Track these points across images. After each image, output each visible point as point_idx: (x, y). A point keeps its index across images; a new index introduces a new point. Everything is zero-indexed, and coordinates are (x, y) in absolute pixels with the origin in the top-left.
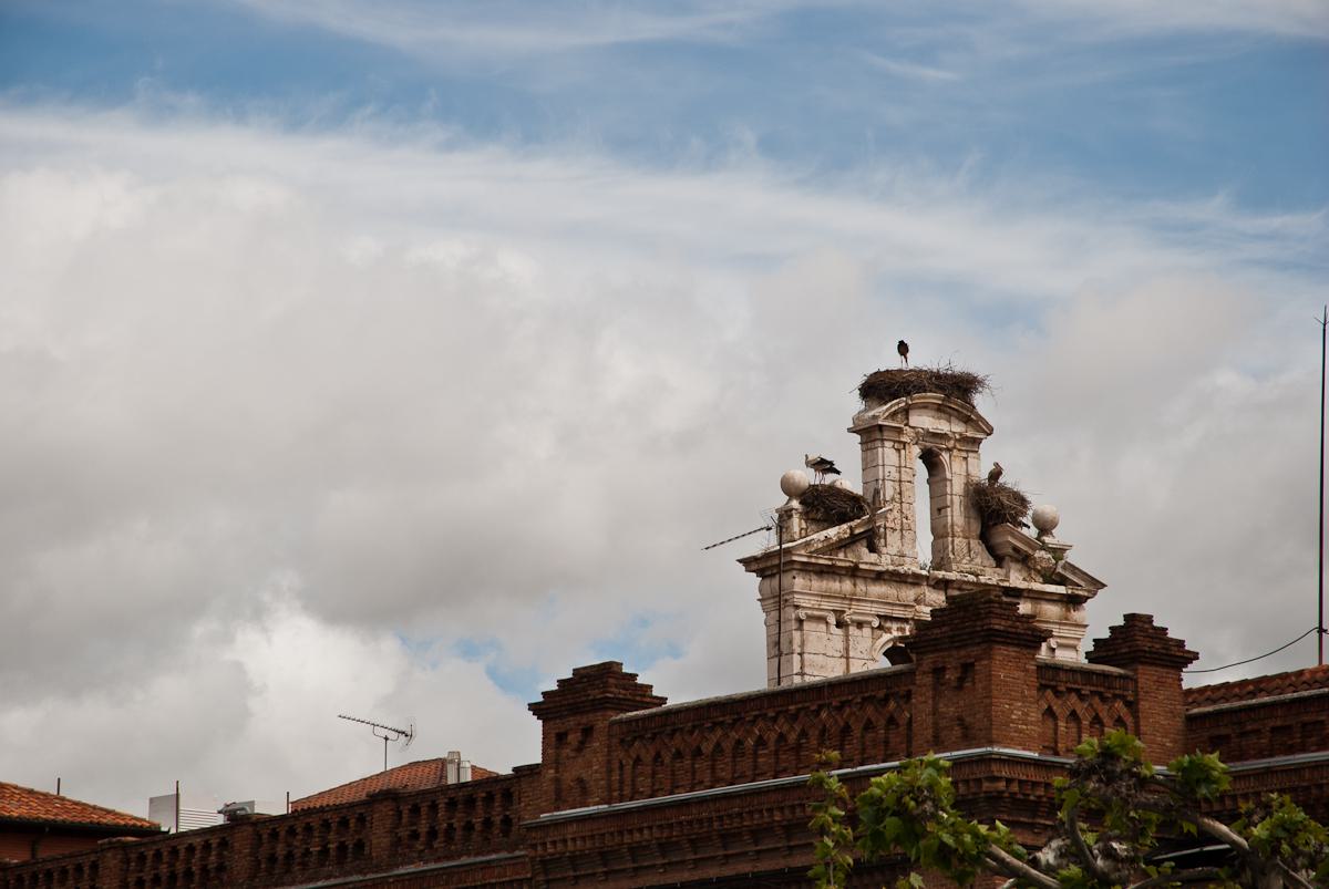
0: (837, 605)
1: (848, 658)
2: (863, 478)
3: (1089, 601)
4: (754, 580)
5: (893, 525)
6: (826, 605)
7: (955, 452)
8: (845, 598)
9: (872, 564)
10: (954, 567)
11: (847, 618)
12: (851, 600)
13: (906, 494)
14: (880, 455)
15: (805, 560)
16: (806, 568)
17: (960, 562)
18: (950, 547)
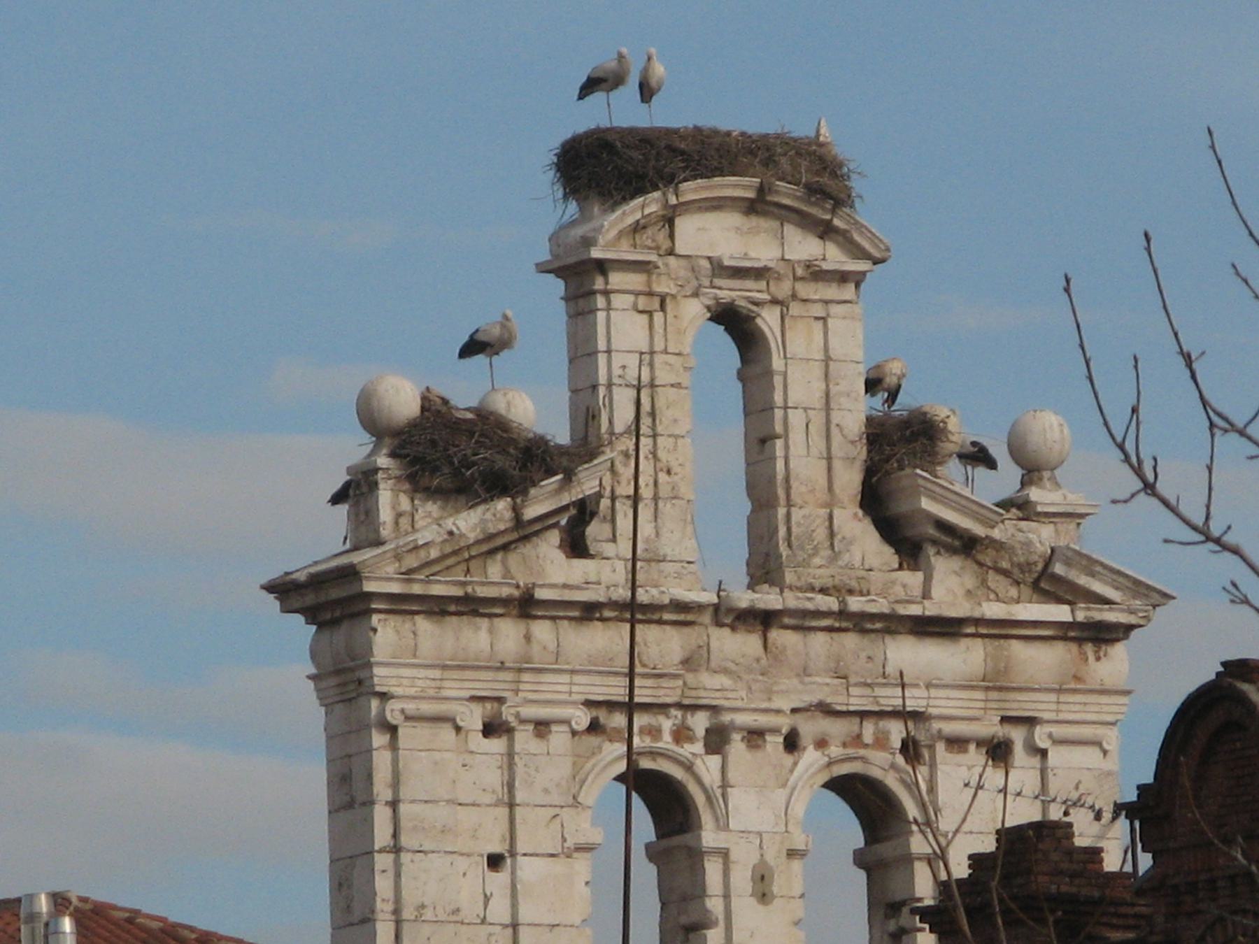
0: (486, 684)
1: (512, 805)
2: (571, 379)
4: (300, 630)
6: (457, 687)
8: (502, 667)
10: (789, 577)
11: (508, 714)
12: (520, 670)
14: (601, 329)
15: (395, 588)
16: (401, 605)
17: (806, 564)
18: (782, 532)
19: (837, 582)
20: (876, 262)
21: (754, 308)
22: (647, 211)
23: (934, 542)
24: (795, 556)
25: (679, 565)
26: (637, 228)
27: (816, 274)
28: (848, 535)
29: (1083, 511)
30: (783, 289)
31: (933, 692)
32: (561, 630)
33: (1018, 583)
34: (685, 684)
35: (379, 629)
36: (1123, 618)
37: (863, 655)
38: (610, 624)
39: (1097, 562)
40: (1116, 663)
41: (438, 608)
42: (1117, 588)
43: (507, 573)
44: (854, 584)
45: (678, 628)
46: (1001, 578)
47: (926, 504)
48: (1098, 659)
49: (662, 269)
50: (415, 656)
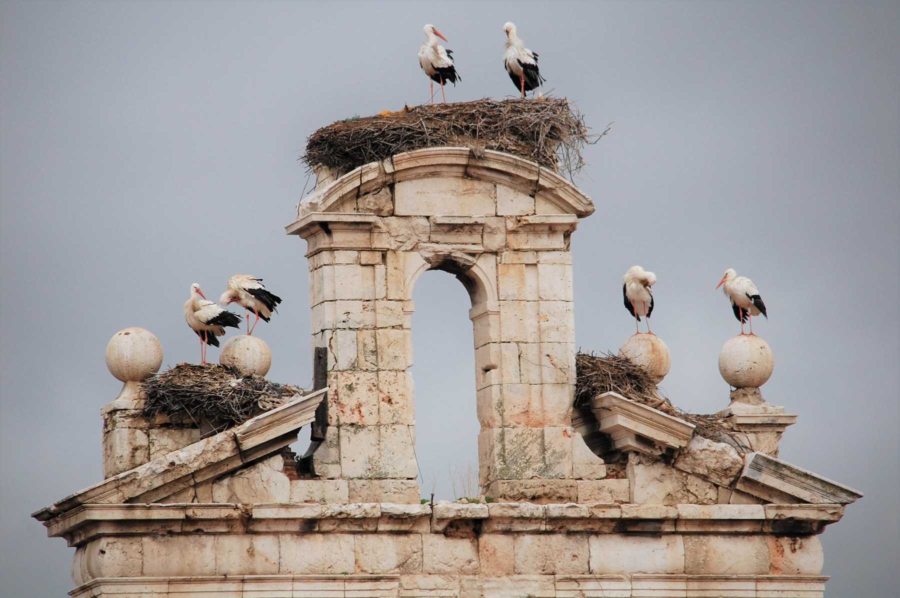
3: (827, 527)
5: (355, 419)
7: (507, 257)
9: (283, 506)
13: (388, 353)
15: (119, 515)
19: (547, 490)
20: (581, 215)
21: (470, 258)
22: (365, 179)
23: (637, 453)
24: (508, 468)
25: (400, 481)
26: (358, 193)
27: (525, 227)
28: (558, 449)
29: (780, 421)
30: (495, 242)
31: (636, 585)
32: (282, 543)
33: (717, 486)
34: (401, 585)
35: (107, 551)
36: (812, 515)
37: (568, 554)
38: (331, 536)
39: (785, 466)
40: (811, 555)
41: (164, 529)
42: (806, 489)
43: (232, 496)
44: (563, 492)
45: (395, 537)
46: (699, 481)
47: (621, 420)
48: (794, 551)
49: (384, 228)
50: (142, 574)
